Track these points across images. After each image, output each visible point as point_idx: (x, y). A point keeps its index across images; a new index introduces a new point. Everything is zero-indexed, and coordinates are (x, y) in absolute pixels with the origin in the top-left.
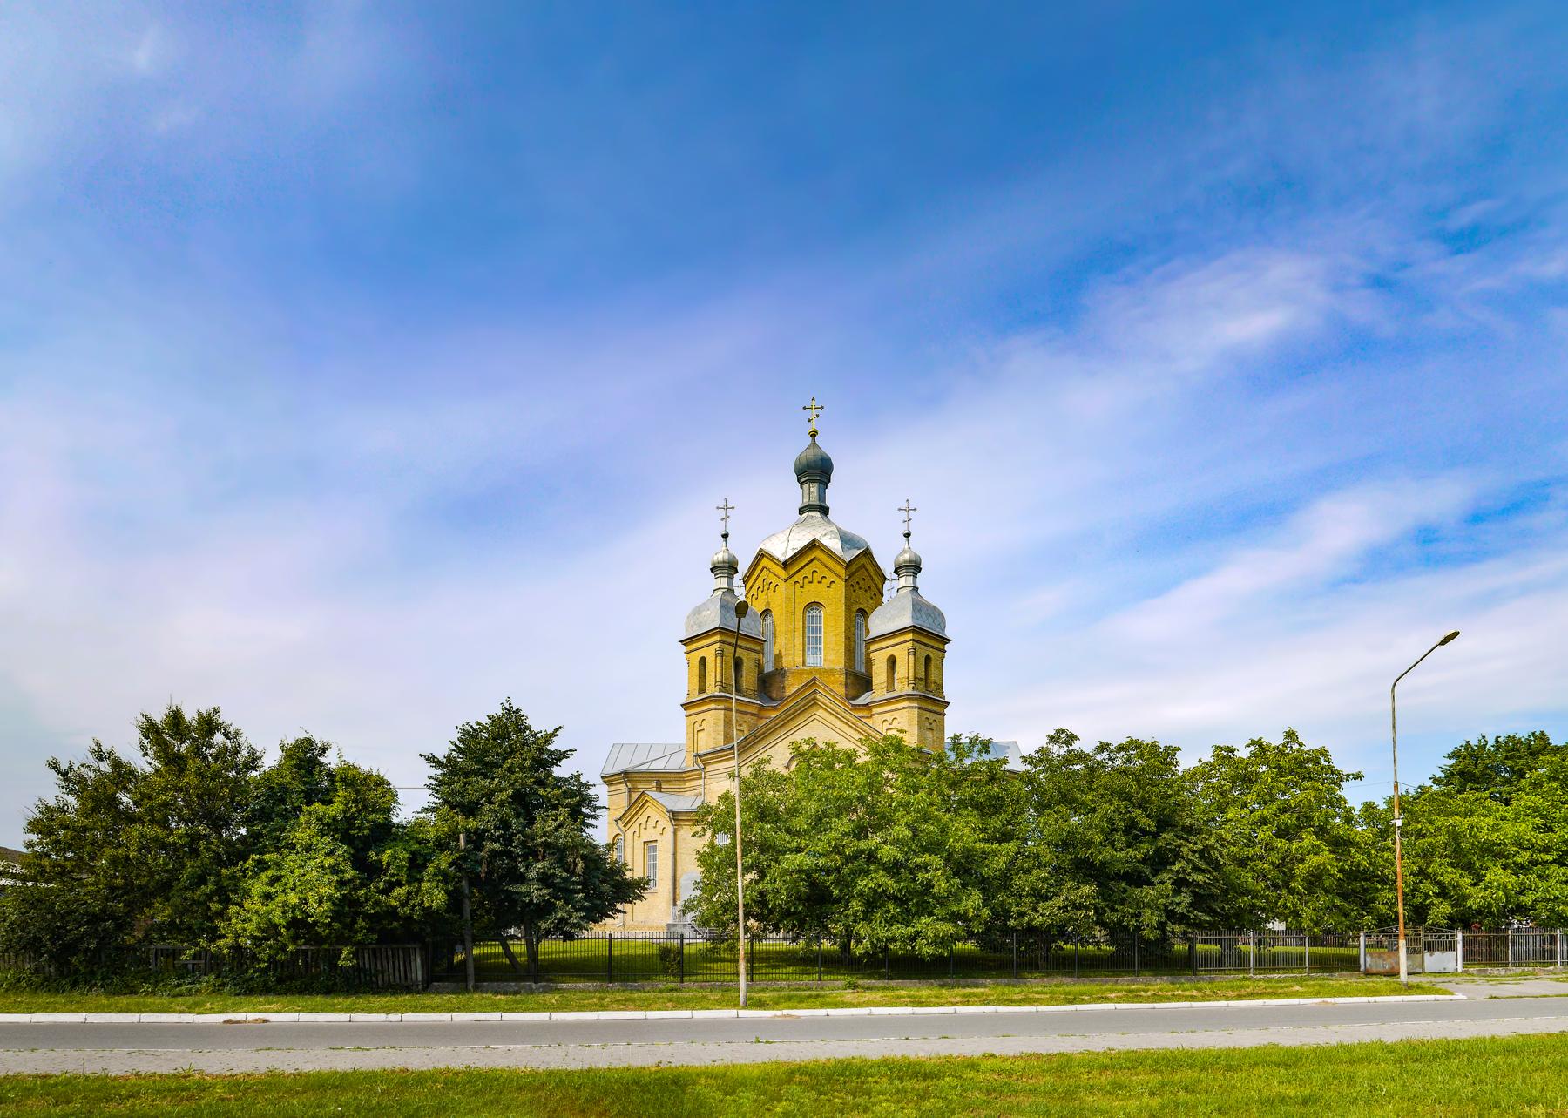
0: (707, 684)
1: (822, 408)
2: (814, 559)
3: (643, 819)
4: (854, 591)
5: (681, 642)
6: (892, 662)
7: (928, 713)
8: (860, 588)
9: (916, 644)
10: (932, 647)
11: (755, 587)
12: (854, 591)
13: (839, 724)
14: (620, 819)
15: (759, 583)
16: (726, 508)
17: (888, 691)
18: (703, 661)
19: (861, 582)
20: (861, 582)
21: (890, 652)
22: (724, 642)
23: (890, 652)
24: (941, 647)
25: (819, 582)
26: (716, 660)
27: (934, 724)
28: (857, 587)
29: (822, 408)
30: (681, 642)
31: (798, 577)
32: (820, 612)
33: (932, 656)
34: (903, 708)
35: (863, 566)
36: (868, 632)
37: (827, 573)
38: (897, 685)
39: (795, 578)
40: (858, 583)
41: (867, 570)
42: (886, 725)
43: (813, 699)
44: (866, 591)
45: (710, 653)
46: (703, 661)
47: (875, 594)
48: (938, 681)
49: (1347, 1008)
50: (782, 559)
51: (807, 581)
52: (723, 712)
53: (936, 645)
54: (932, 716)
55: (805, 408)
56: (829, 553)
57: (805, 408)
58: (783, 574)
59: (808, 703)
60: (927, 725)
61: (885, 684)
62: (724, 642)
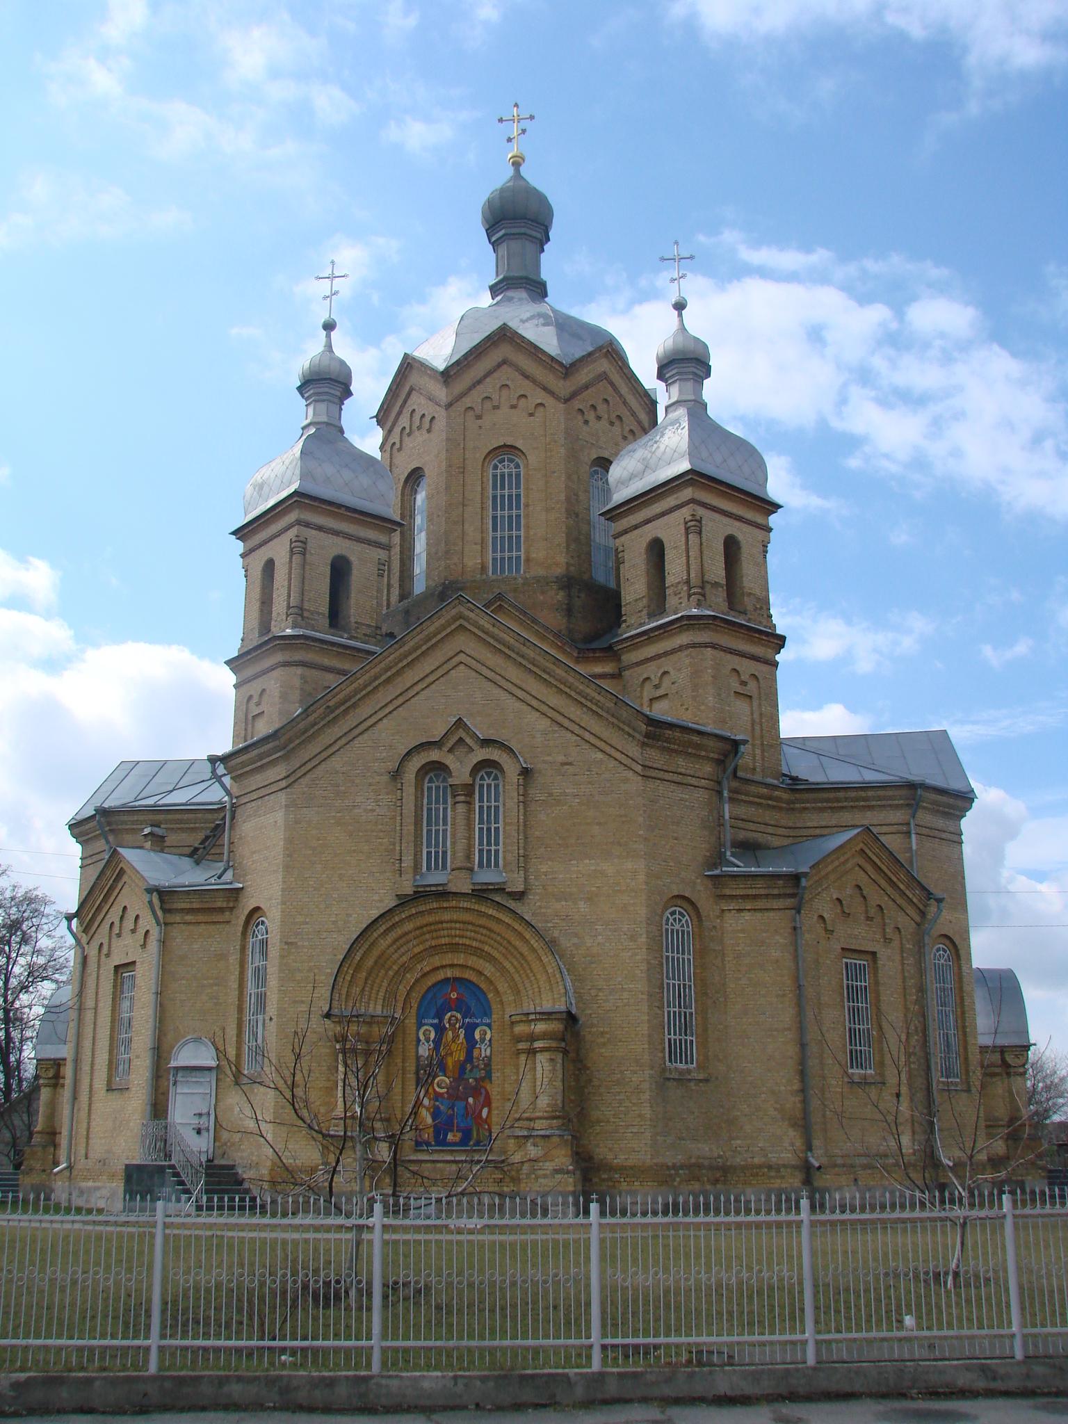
0: (274, 614)
1: (532, 118)
2: (505, 362)
3: (114, 915)
4: (586, 422)
5: (234, 533)
6: (657, 549)
7: (736, 659)
8: (599, 418)
9: (701, 511)
10: (739, 519)
11: (397, 430)
12: (586, 422)
13: (513, 673)
14: (76, 915)
15: (404, 421)
16: (332, 277)
17: (652, 616)
18: (270, 565)
19: (602, 408)
20: (602, 408)
21: (650, 532)
22: (307, 525)
23: (650, 532)
24: (759, 519)
25: (513, 407)
26: (291, 561)
27: (752, 685)
28: (591, 416)
29: (532, 118)
30: (234, 533)
31: (474, 399)
32: (517, 466)
33: (740, 537)
34: (681, 648)
35: (604, 377)
36: (607, 492)
37: (526, 387)
38: (671, 601)
39: (467, 402)
40: (594, 407)
41: (612, 384)
42: (648, 692)
43: (455, 619)
44: (612, 424)
45: (279, 551)
46: (270, 565)
47: (619, 417)
48: (757, 592)
49: (487, 860)
50: (441, 366)
51: (488, 405)
52: (299, 670)
53: (749, 515)
54: (747, 667)
55: (501, 120)
56: (533, 351)
57: (501, 120)
58: (441, 393)
59: (444, 627)
60: (736, 685)
61: (645, 601)
62: (307, 525)
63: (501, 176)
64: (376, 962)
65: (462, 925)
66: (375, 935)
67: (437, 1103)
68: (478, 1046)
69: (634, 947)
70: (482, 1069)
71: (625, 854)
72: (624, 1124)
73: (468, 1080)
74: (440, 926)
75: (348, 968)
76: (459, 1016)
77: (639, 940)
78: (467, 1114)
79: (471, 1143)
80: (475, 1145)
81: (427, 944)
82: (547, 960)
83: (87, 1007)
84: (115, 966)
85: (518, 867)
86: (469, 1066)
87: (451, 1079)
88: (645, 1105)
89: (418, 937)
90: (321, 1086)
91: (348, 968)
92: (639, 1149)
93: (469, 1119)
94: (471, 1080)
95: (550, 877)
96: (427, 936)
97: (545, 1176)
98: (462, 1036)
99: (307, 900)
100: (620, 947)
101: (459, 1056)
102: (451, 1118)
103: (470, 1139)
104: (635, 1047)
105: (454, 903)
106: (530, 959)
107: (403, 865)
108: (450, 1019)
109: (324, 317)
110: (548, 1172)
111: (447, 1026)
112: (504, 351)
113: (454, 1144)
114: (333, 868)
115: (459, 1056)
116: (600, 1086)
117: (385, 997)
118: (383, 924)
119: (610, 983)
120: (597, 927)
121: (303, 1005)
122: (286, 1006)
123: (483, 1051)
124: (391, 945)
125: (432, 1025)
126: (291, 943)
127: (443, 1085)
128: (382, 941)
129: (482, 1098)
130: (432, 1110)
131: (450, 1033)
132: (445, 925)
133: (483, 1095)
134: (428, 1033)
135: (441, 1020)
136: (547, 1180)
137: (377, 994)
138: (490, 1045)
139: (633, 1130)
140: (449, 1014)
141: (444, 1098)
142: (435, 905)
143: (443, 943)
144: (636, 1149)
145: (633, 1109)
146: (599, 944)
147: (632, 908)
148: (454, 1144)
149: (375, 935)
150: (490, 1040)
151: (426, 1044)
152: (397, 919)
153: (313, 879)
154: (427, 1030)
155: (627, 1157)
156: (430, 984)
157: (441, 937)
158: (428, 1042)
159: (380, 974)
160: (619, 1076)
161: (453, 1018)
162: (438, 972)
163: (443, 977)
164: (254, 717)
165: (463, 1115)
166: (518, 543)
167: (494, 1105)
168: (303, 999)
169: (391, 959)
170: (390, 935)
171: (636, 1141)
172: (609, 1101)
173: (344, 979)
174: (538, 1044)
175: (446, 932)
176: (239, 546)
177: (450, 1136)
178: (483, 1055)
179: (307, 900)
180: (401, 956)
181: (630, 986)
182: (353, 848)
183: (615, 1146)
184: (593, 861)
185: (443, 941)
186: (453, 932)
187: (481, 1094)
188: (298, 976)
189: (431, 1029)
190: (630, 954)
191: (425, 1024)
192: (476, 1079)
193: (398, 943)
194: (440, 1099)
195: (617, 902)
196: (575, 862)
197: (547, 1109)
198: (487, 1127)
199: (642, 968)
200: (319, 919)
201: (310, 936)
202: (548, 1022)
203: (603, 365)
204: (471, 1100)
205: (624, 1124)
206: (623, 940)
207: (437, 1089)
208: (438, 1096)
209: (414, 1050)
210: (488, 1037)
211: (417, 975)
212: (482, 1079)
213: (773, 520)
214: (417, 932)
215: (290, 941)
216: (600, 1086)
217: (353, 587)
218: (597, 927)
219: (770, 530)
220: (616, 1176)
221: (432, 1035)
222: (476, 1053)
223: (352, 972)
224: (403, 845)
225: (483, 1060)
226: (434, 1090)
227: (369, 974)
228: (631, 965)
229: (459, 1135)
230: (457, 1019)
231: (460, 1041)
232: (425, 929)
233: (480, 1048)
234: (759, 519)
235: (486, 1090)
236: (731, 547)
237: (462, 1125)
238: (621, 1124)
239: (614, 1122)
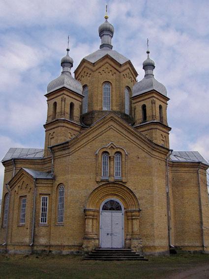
6: (144, 107)
18: (55, 104)
24: (167, 131)
46: (55, 104)
54: (164, 134)
63: (103, 22)
84: (130, 61)
109: (67, 48)
112: (107, 60)
164: (51, 138)
166: (42, 215)
176: (46, 99)
203: (128, 66)
213: (168, 102)
217: (75, 107)
219: (167, 104)
234: (167, 131)
236: (160, 107)
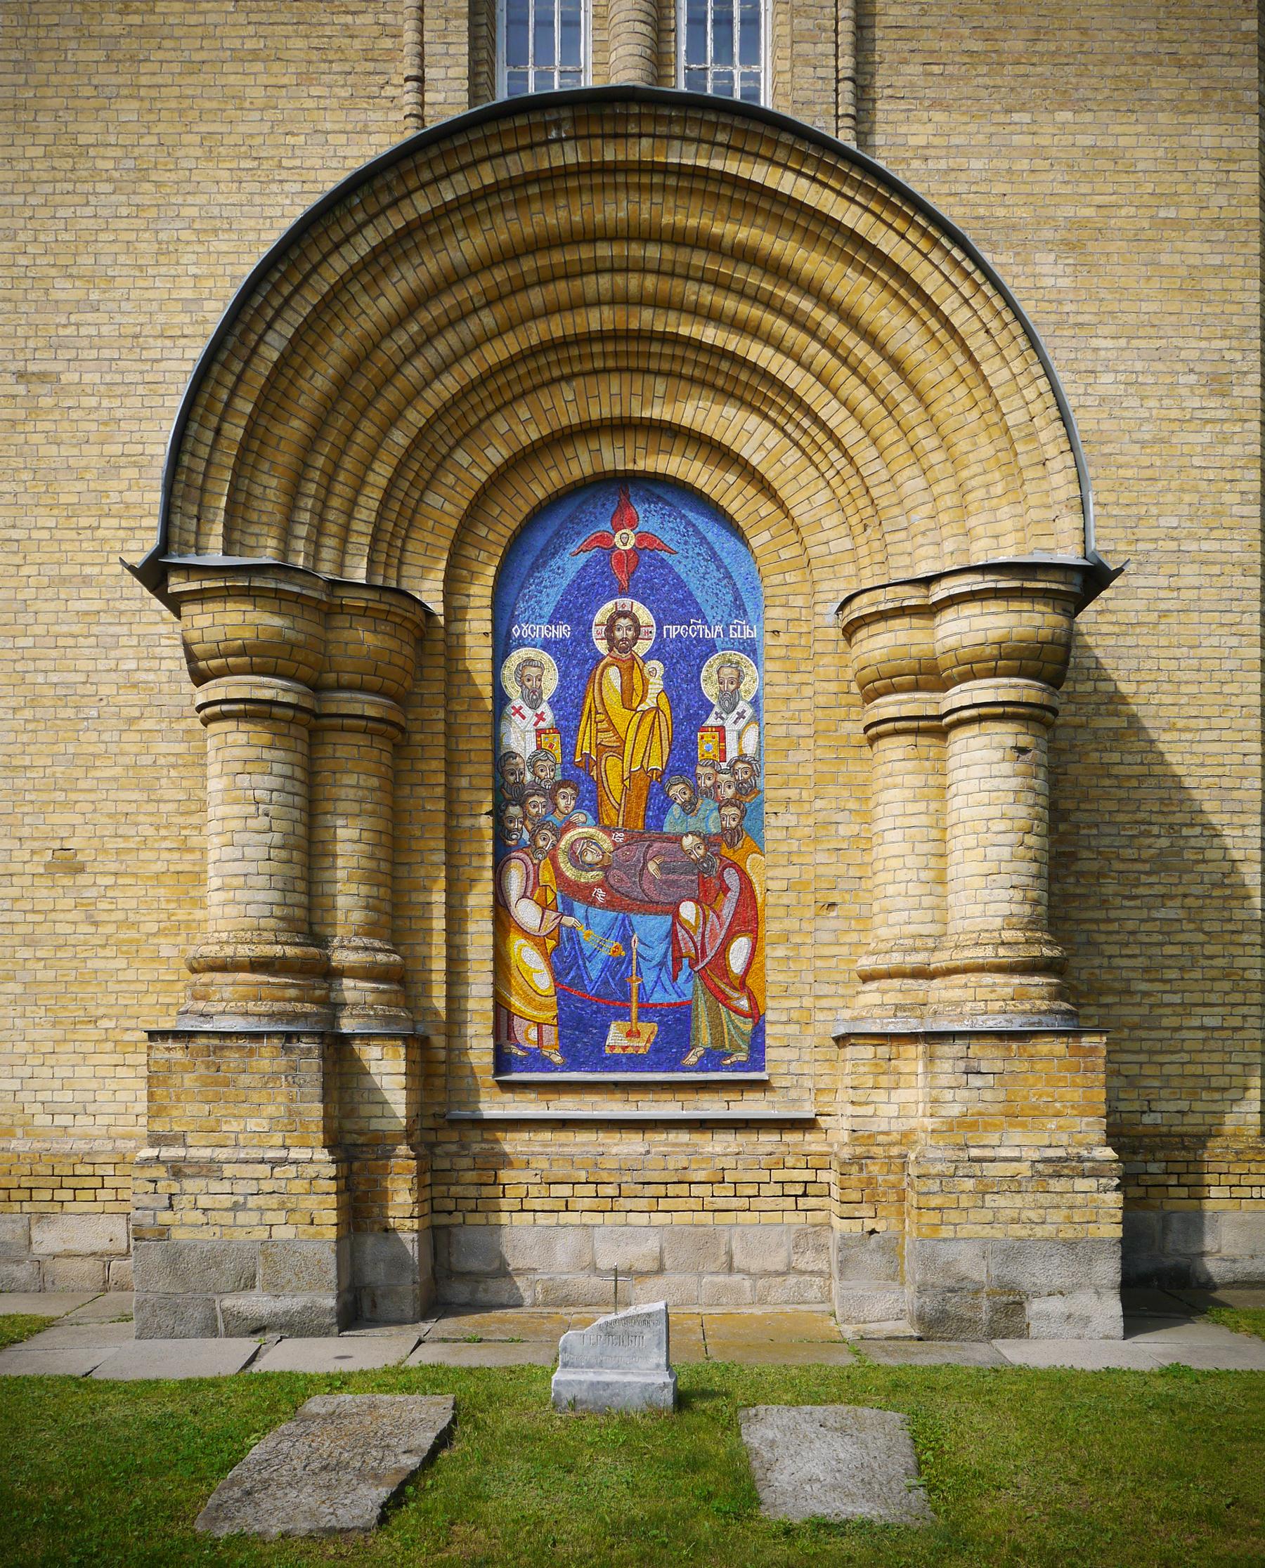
64: (342, 384)
65: (668, 253)
66: (339, 266)
67: (568, 921)
68: (712, 721)
69: (1221, 414)
70: (729, 803)
71: (1193, 95)
72: (1176, 999)
73: (678, 839)
74: (585, 252)
75: (233, 393)
76: (644, 615)
77: (1236, 391)
78: (677, 961)
79: (692, 1059)
80: (700, 1068)
81: (537, 332)
82: (1005, 374)
83: (267, 1057)
85: (837, 117)
86: (677, 791)
87: (620, 837)
88: (1245, 938)
89: (501, 298)
90: (160, 867)
91: (233, 393)
92: (1224, 1082)
93: (682, 977)
94: (688, 841)
95: (942, 164)
96: (536, 297)
97: (1014, 1185)
98: (656, 685)
99: (90, 223)
100: (1174, 414)
101: (647, 754)
102: (618, 967)
103: (687, 1045)
104: (1216, 747)
105: (642, 150)
106: (927, 377)
107: (429, 97)
108: (611, 626)
110: (1024, 1169)
111: (602, 646)
113: (634, 1062)
114: (181, 112)
115: (647, 754)
116: (1100, 874)
117: (377, 528)
118: (370, 220)
119: (1141, 533)
120: (1095, 343)
121: (85, 592)
122: (29, 594)
123: (731, 737)
124: (398, 321)
125: (547, 645)
126: (42, 377)
127: (589, 858)
128: (364, 300)
129: (728, 908)
130: (551, 944)
131: (613, 673)
132: (603, 250)
133: (733, 895)
134: (532, 671)
135: (583, 637)
136: (1018, 1200)
137: (350, 516)
138: (756, 719)
139: (1209, 1022)
140: (609, 606)
141: (592, 903)
142: (571, 155)
143: (595, 326)
144: (1215, 1083)
145: (1209, 950)
146: (1103, 399)
147: (1215, 284)
148: (634, 1062)
149: (339, 266)
150: (755, 703)
151: (527, 711)
152: (422, 204)
153: (110, 152)
154: (529, 662)
155: (1183, 1105)
156: (541, 494)
157: (588, 305)
158: (534, 705)
159: (359, 438)
160: (1164, 842)
161: (624, 622)
162: (569, 452)
163: (588, 471)
165: (662, 964)
167: (771, 927)
168: (88, 570)
169: (400, 381)
170: (396, 276)
171: (1217, 1057)
172: (1130, 926)
173: (218, 431)
174: (959, 696)
175: (605, 281)
177: (616, 1037)
178: (732, 754)
179: (90, 223)
180: (437, 374)
181: (1206, 546)
182: (250, 44)
183: (1147, 1070)
184: (1088, 117)
185: (594, 320)
186: (634, 281)
187: (726, 890)
188: (69, 492)
189: (546, 657)
190: (1206, 438)
191: (521, 643)
192: (708, 840)
193: (425, 317)
194: (579, 908)
195: (1165, 259)
196: (1026, 118)
197: (1008, 935)
198: (744, 1004)
199: (1243, 486)
200: (134, 294)
201: (106, 353)
202: (1015, 605)
204: (688, 911)
205: (1176, 999)
206: (1184, 391)
207: (570, 872)
208: (573, 894)
209: (487, 731)
210: (749, 687)
211: (497, 455)
212: (731, 836)
214: (499, 275)
215: (32, 367)
216: (1100, 874)
218: (1095, 343)
220: (1153, 1168)
221: (550, 682)
222: (706, 745)
223: (248, 408)
224: (428, 24)
225: (732, 770)
226: (559, 874)
227: (318, 429)
228: (1211, 474)
229: (648, 1030)
230: (637, 627)
231: (650, 702)
232: (527, 264)
233: (721, 729)
235: (742, 874)
237: (658, 997)
238: (1168, 998)
239: (1146, 994)
